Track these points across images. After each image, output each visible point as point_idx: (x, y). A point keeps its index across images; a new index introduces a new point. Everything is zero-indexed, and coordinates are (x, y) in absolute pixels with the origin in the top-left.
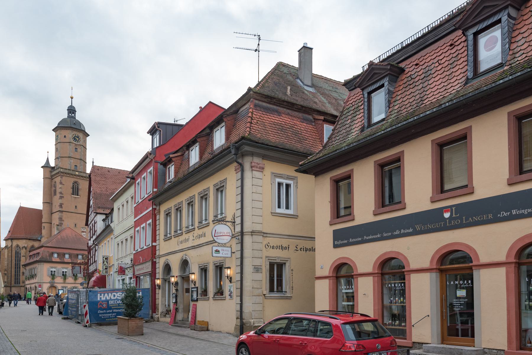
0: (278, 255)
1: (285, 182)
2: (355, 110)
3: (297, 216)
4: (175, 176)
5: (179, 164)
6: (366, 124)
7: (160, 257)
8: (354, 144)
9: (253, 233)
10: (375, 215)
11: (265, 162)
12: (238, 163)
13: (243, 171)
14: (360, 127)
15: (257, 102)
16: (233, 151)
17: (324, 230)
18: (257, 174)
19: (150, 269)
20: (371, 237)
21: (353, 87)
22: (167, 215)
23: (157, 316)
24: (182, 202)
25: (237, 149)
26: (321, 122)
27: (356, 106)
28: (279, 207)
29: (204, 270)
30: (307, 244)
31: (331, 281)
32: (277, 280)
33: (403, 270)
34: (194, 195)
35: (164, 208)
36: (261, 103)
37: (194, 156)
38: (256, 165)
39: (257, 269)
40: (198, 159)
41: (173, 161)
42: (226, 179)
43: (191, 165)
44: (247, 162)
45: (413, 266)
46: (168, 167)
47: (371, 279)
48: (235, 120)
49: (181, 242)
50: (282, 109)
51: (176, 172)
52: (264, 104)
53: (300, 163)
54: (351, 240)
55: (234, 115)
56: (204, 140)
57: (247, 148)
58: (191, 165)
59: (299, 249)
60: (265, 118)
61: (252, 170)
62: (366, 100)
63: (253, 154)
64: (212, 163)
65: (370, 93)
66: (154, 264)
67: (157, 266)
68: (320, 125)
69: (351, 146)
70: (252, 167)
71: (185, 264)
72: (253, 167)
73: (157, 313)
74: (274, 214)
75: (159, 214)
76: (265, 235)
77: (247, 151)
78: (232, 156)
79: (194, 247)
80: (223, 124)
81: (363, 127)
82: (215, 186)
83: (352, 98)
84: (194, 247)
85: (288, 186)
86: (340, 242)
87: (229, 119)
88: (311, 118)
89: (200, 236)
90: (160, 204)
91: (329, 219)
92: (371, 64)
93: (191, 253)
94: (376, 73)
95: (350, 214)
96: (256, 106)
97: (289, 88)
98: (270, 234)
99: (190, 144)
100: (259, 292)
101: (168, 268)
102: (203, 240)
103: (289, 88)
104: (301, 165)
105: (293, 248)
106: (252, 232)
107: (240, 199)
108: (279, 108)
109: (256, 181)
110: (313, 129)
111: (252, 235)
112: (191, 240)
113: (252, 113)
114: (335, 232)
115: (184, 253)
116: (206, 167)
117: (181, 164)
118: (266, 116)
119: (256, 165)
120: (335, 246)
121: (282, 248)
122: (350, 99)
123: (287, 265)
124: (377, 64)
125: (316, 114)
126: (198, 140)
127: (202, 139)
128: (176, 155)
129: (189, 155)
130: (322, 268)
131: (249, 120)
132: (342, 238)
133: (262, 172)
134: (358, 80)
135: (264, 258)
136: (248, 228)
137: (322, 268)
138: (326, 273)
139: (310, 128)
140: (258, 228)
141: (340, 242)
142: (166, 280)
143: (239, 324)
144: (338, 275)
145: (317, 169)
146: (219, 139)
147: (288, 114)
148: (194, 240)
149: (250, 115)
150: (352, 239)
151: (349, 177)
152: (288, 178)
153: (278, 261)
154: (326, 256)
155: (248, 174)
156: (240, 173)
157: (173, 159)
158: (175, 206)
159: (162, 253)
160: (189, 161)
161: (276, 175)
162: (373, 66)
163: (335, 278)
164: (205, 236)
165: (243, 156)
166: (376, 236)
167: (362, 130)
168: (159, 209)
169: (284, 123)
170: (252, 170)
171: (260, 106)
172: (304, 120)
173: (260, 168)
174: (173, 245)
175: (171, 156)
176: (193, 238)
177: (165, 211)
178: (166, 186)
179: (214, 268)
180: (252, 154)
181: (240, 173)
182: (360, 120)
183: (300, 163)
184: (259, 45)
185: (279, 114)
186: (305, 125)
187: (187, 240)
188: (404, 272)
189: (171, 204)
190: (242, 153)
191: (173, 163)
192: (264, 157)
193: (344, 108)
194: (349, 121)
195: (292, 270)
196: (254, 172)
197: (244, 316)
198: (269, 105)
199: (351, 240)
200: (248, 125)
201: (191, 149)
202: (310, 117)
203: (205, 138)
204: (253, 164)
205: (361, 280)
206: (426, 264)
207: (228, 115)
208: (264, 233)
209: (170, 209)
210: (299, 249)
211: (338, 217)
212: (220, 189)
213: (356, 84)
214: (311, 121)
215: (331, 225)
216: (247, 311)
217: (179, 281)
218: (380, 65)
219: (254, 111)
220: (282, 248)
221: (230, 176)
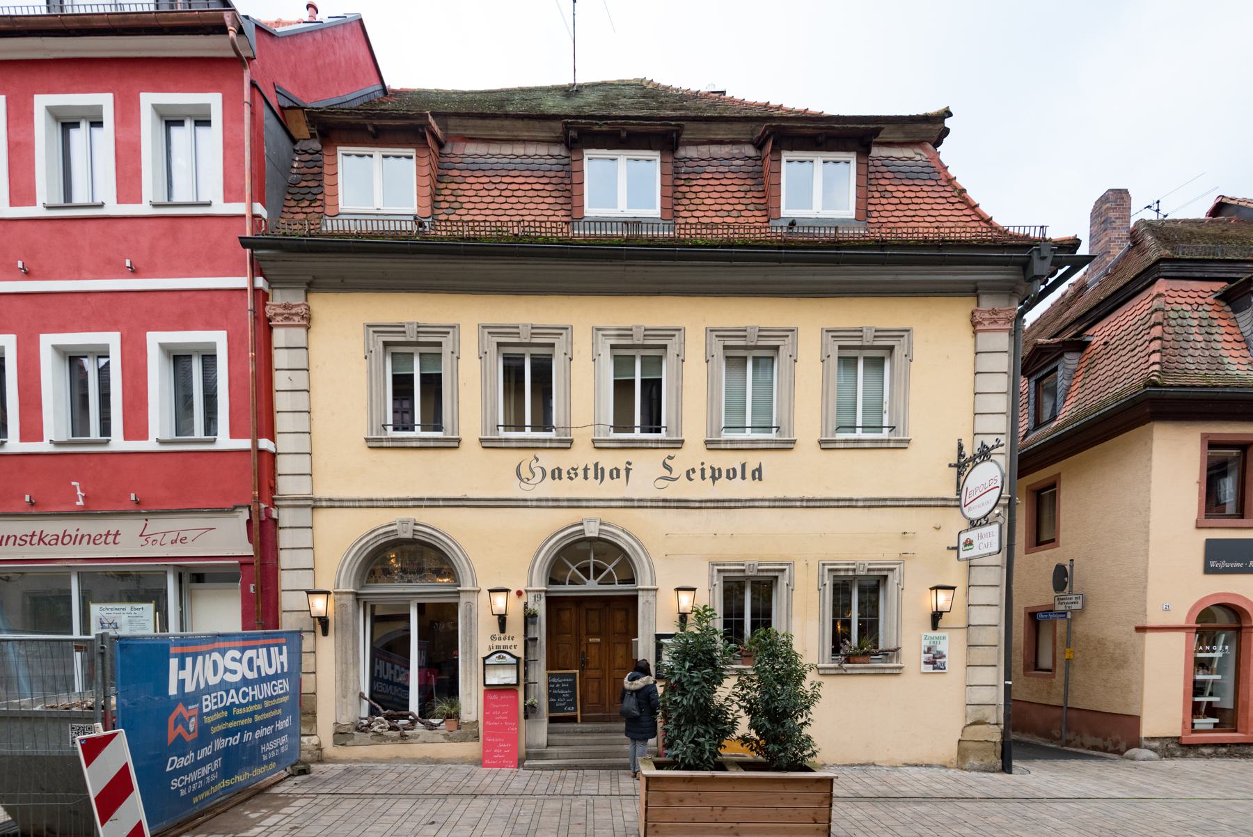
47: (1182, 636)
114: (1209, 543)
120: (1208, 570)
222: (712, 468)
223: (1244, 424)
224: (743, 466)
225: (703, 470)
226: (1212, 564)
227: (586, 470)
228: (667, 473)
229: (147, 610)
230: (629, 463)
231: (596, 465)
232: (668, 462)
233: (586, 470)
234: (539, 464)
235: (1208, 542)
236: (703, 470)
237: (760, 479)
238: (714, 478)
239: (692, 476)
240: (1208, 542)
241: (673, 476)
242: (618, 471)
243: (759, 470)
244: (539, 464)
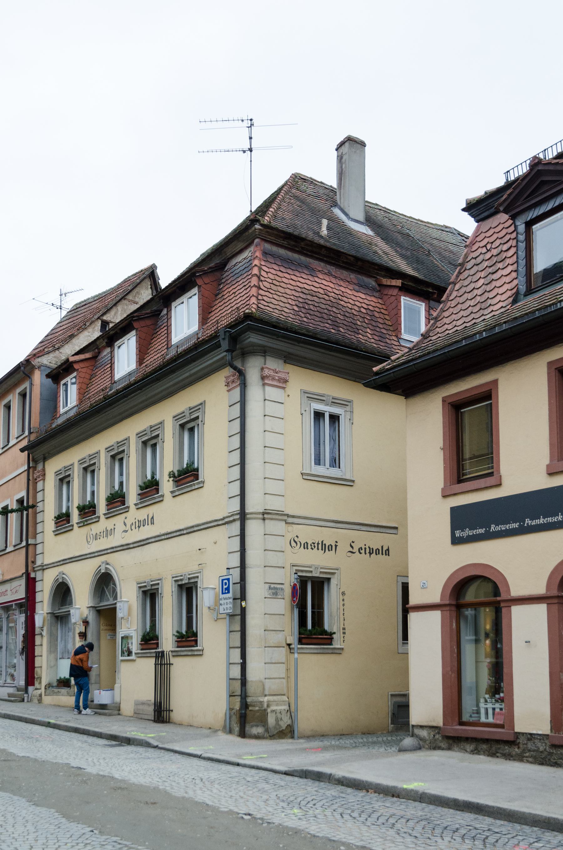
0: (315, 562)
1: (328, 409)
2: (495, 259)
3: (353, 481)
4: (81, 401)
5: (88, 376)
6: (523, 289)
7: (44, 568)
8: (504, 327)
9: (265, 515)
10: (551, 474)
11: (290, 368)
12: (235, 368)
13: (244, 386)
14: (509, 293)
15: (268, 246)
16: (225, 345)
17: (429, 508)
18: (272, 393)
19: (21, 594)
20: (542, 521)
21: (492, 210)
22: (61, 480)
23: (39, 692)
24: (98, 453)
25: (234, 339)
26: (395, 292)
27: (495, 252)
28: (318, 461)
29: (150, 595)
30: (383, 536)
31: (447, 614)
32: (313, 613)
33: (498, 599)
34: (128, 439)
35: (53, 466)
36: (275, 249)
37: (125, 359)
38: (272, 373)
39: (274, 591)
40: (133, 366)
41: (75, 370)
42: (203, 404)
43: (117, 376)
44: (253, 368)
45: (516, 591)
46: (63, 382)
47: (437, 615)
48: (219, 282)
49: (96, 537)
50: (316, 263)
51: (82, 394)
52: (282, 252)
53: (375, 369)
54: (493, 528)
55: (218, 274)
56: (147, 326)
57: (253, 338)
58: (117, 376)
59: (356, 549)
60: (284, 280)
61: (264, 385)
62: (522, 238)
63: (265, 352)
64: (166, 375)
65: (529, 224)
66: (31, 585)
67: (38, 588)
68: (393, 298)
69: (497, 330)
70: (263, 378)
71: (104, 582)
72: (267, 377)
73: (37, 685)
74: (306, 476)
75: (44, 480)
76: (290, 520)
77: (253, 345)
78: (220, 355)
79: (126, 547)
80: (195, 290)
81: (517, 293)
82: (176, 418)
83: (483, 235)
84: (126, 547)
85: (334, 418)
86: (468, 532)
87: (207, 280)
88: (374, 283)
89: (140, 524)
90: (45, 459)
91: (440, 484)
92: (536, 163)
93: (113, 558)
94: (543, 183)
95: (491, 474)
96: (265, 253)
97: (325, 222)
98: (299, 517)
99: (116, 333)
100: (279, 638)
101: (63, 592)
102: (147, 532)
103: (325, 222)
104: (377, 373)
105: (344, 547)
106: (263, 514)
107: (238, 445)
108: (311, 261)
109: (271, 408)
110: (378, 305)
111: (264, 519)
112: (118, 529)
113: (260, 269)
114: (454, 511)
115: (103, 558)
116: (158, 379)
117: (92, 377)
118: (286, 275)
119: (272, 373)
120: (456, 541)
121: (324, 547)
122: (478, 239)
123: (333, 582)
124: (549, 164)
125: (385, 277)
126: (135, 324)
127: (142, 323)
128: (82, 357)
129: (112, 357)
130: (424, 587)
131: (254, 281)
132: (468, 524)
133: (284, 388)
134: (509, 192)
135: (288, 567)
136: (254, 505)
137: (424, 587)
138: (435, 597)
139: (372, 303)
140: (275, 504)
141: (468, 532)
142: (60, 619)
143: (237, 706)
144: (462, 601)
145: (410, 380)
146: (185, 321)
147: (329, 274)
148: (126, 531)
149: (255, 271)
150: (497, 525)
151: (487, 396)
152: (335, 402)
153: (316, 574)
154: (434, 560)
155: (255, 392)
156: (238, 390)
157: (76, 366)
158: (81, 462)
159: (48, 560)
160: (112, 368)
161: (312, 397)
162: (540, 167)
163: (454, 608)
164: (152, 523)
165: (245, 354)
166: (555, 519)
167: (426, 325)
168: (44, 470)
169: (322, 291)
170: (264, 385)
171: (273, 255)
172: (362, 286)
173: (279, 380)
174: (77, 540)
175: (72, 359)
176: (124, 528)
177: (57, 473)
178: (60, 421)
179: (175, 589)
180: (264, 352)
181: (237, 391)
182: (508, 279)
183: (375, 369)
184: (251, 138)
185: (312, 272)
186: (363, 296)
187: (108, 533)
188: (499, 602)
189: (72, 458)
190: (242, 349)
191: (75, 374)
192: (289, 358)
193: (466, 256)
194: (481, 281)
195: (343, 594)
196: (267, 388)
197: (251, 688)
198: (290, 254)
199: (493, 528)
200: (254, 291)
201: (117, 343)
202: (372, 282)
203: (148, 322)
204: (266, 372)
205: (517, 611)
206: (541, 589)
207: (205, 273)
208: (288, 516)
209: (69, 468)
210: (356, 549)
211: (460, 481)
212: (189, 425)
213: (501, 204)
214: (374, 289)
215: (444, 497)
216: (254, 679)
217: (91, 619)
218: (557, 163)
219: (263, 263)
220: (324, 547)
221: (213, 396)
222: (369, 547)
223: (474, 377)
224: (382, 547)
225: (365, 548)
226: (458, 534)
227: (318, 544)
228: (351, 549)
229: (34, 540)
230: (336, 542)
231: (322, 542)
232: (352, 544)
233: (318, 544)
234: (299, 540)
235: (453, 510)
236: (365, 548)
237: (389, 555)
238: (370, 554)
239: (361, 551)
240: (453, 510)
241: (354, 551)
242: (332, 546)
243: (388, 550)
244: (299, 540)
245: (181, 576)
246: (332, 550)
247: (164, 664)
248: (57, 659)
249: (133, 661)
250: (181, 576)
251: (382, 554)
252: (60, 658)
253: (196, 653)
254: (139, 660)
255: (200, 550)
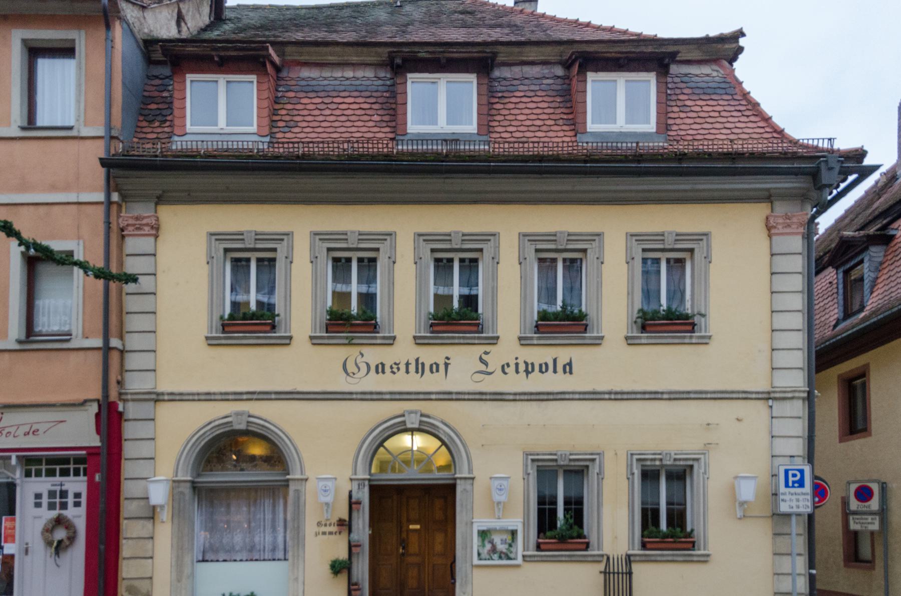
33: (288, 477)
222: (526, 363)
224: (555, 361)
225: (517, 365)
227: (407, 364)
230: (448, 358)
232: (484, 357)
233: (407, 364)
234: (364, 359)
236: (517, 365)
237: (571, 373)
238: (527, 372)
239: (507, 370)
241: (489, 370)
242: (437, 365)
243: (570, 364)
244: (364, 359)
245: (660, 454)
246: (437, 371)
247: (614, 573)
248: (193, 564)
249: (518, 566)
250: (660, 454)
251: (555, 371)
252: (199, 561)
253: (695, 559)
254: (529, 567)
255: (708, 424)
